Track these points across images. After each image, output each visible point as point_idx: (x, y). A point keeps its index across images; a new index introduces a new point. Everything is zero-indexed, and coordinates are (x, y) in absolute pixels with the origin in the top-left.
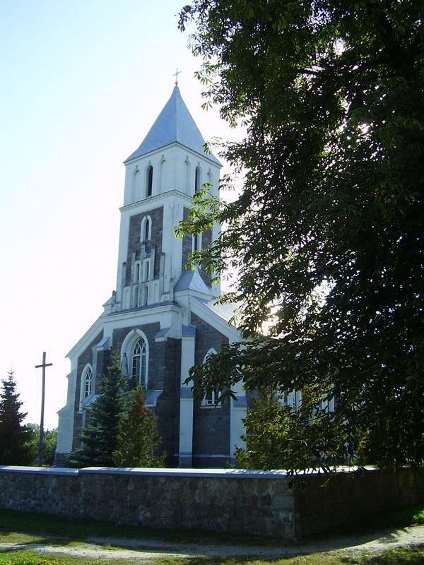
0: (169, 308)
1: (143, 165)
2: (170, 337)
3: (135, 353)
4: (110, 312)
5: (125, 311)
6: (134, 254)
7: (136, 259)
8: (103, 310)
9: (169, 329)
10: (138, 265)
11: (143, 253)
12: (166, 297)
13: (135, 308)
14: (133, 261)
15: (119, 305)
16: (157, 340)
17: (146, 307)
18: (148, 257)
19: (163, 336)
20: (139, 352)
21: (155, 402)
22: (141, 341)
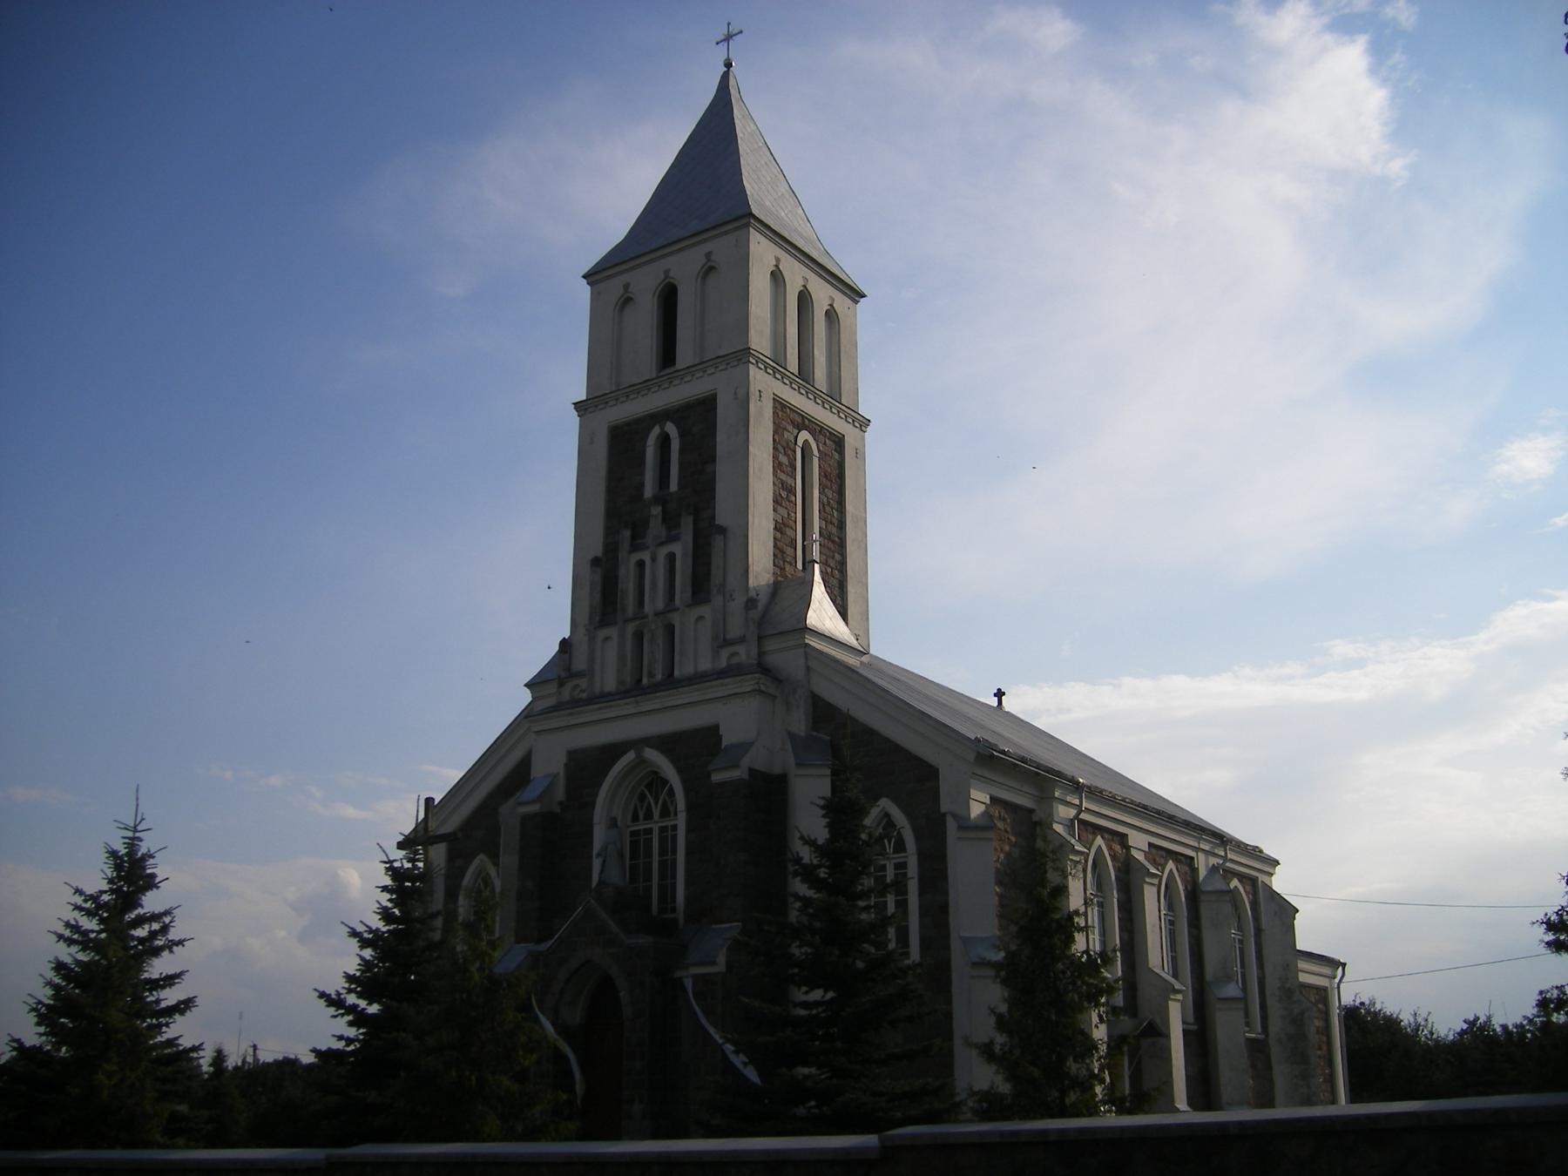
0: (748, 683)
1: (646, 283)
2: (757, 767)
3: (635, 818)
4: (552, 701)
5: (602, 698)
6: (627, 533)
7: (635, 547)
8: (526, 697)
9: (751, 744)
10: (641, 564)
11: (656, 528)
12: (577, 686)
13: (634, 689)
14: (622, 554)
15: (583, 683)
16: (716, 777)
17: (671, 682)
18: (671, 539)
19: (736, 766)
20: (649, 816)
21: (722, 959)
22: (656, 782)
